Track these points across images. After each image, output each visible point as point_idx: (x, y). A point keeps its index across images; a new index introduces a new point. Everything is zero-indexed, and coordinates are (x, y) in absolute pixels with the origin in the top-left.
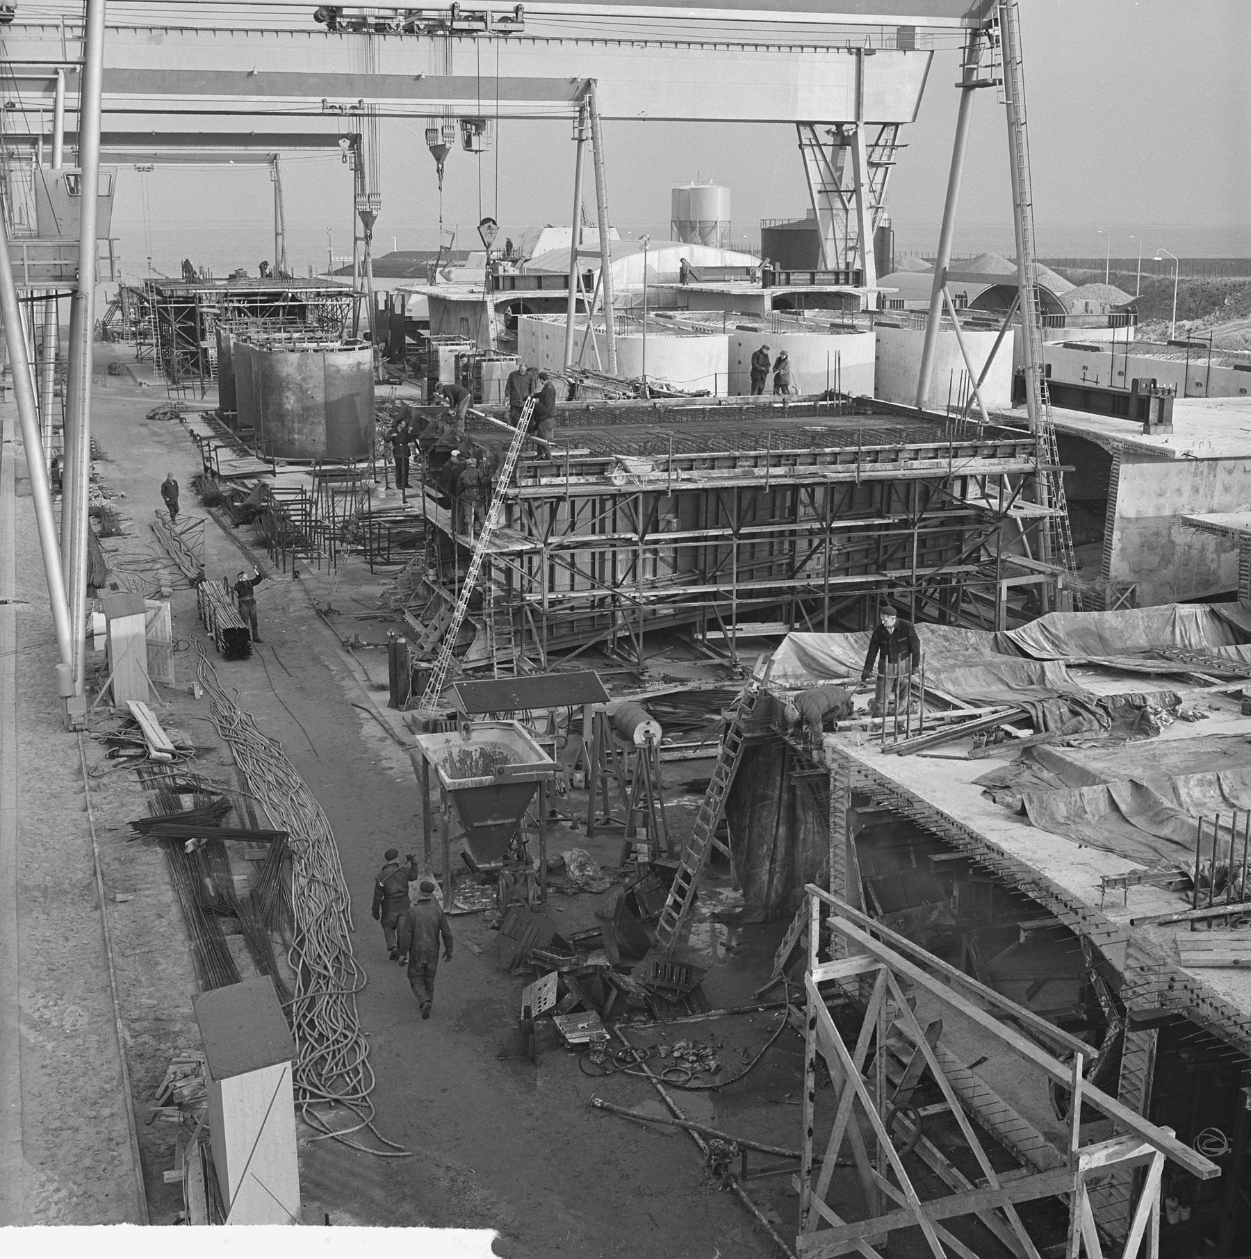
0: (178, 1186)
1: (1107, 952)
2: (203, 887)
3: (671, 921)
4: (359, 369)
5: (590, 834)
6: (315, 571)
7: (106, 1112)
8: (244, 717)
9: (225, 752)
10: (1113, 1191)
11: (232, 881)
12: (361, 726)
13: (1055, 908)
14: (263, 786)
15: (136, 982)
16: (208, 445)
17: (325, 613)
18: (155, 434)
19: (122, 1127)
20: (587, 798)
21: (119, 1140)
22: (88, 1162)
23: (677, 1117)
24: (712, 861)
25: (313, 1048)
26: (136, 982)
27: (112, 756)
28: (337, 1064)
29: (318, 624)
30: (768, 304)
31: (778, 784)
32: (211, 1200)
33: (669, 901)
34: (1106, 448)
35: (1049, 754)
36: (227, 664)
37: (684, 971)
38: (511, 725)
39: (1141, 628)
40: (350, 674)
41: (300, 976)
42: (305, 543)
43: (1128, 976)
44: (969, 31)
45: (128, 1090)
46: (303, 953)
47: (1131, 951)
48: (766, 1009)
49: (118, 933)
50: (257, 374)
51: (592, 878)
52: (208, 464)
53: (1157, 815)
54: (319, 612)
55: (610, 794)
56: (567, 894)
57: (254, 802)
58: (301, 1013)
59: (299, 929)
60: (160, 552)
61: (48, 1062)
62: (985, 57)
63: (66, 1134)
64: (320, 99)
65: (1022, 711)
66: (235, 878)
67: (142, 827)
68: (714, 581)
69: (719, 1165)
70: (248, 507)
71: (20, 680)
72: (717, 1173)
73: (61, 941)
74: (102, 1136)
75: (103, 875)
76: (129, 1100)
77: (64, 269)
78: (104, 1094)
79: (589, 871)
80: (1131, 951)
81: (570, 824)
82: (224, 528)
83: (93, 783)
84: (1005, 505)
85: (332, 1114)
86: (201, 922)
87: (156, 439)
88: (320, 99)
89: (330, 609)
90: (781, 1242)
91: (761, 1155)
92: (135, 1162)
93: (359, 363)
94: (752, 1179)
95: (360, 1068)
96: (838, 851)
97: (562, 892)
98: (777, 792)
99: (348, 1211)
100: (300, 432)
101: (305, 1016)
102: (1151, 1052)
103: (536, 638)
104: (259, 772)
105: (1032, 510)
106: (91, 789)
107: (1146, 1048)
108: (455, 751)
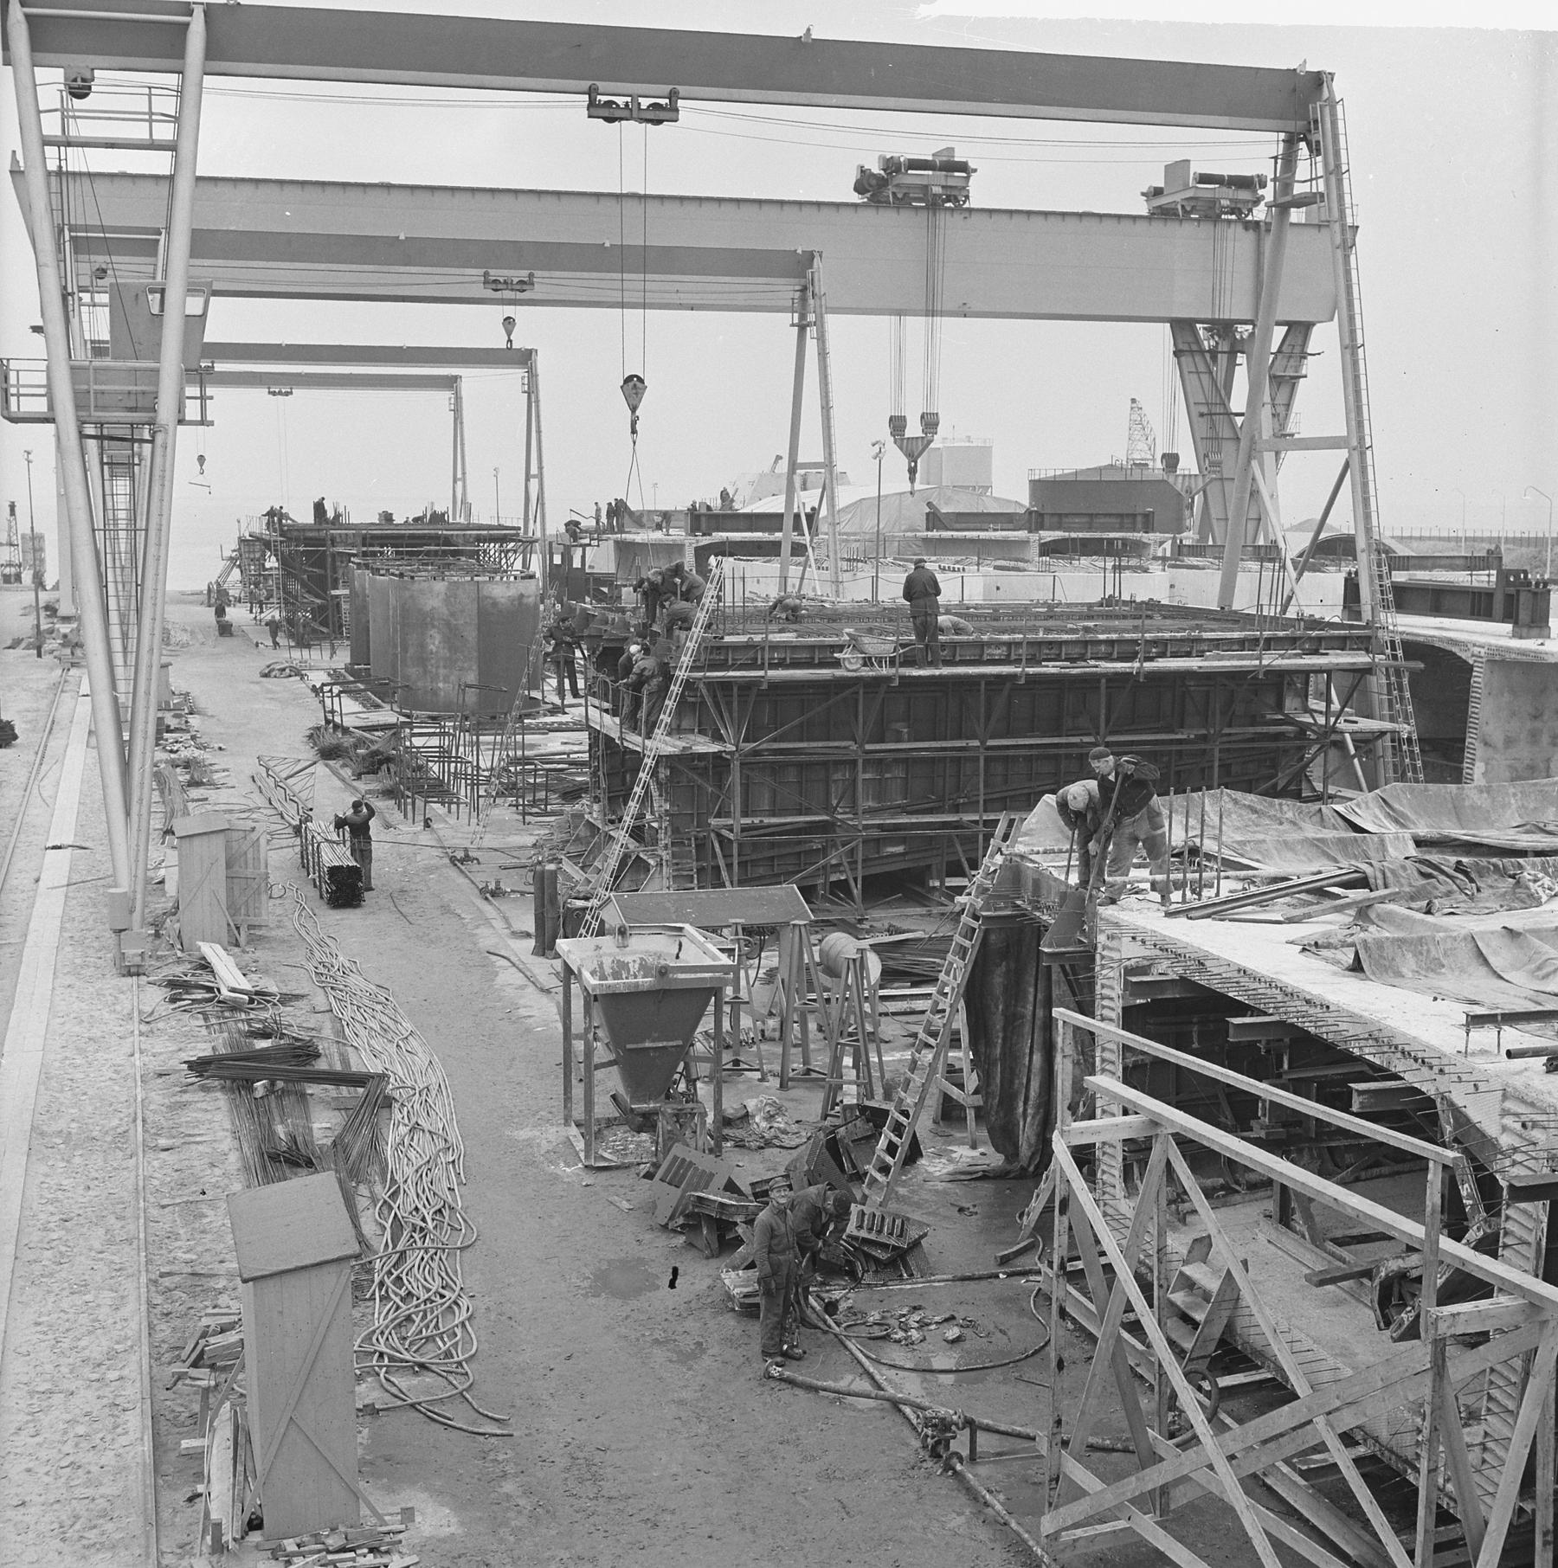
0: (197, 1456)
1: (1474, 1115)
2: (272, 1133)
3: (884, 1169)
4: (520, 604)
5: (783, 1086)
6: (452, 820)
7: (113, 1375)
8: (347, 964)
9: (320, 1001)
10: (1487, 1456)
11: (311, 1129)
12: (497, 974)
13: (1398, 1066)
14: (363, 1033)
15: (173, 1236)
16: (331, 691)
17: (462, 861)
18: (269, 691)
19: (133, 1391)
20: (779, 1050)
21: (126, 1405)
22: (81, 1430)
23: (880, 1388)
24: (943, 1118)
25: (398, 1308)
26: (173, 1236)
27: (173, 1000)
28: (427, 1327)
29: (452, 873)
30: (1035, 550)
31: (1031, 998)
32: (240, 1468)
33: (882, 1143)
34: (1463, 655)
35: (1390, 913)
36: (331, 912)
37: (898, 1222)
38: (681, 929)
39: (1514, 807)
40: (487, 922)
41: (389, 1230)
42: (439, 791)
43: (1505, 1141)
44: (1282, 136)
45: (145, 1349)
46: (395, 1206)
47: (1509, 1105)
48: (1010, 1275)
49: (156, 1182)
50: (395, 609)
51: (785, 1132)
52: (330, 716)
53: (1539, 968)
54: (453, 860)
55: (812, 1046)
56: (749, 1148)
57: (350, 1049)
58: (386, 1269)
59: (393, 1181)
60: (260, 801)
61: (44, 1319)
62: (1303, 170)
63: (57, 1399)
64: (481, 272)
65: (1356, 872)
66: (315, 1126)
67: (200, 1067)
68: (956, 809)
69: (938, 1443)
70: (376, 753)
71: (67, 925)
72: (935, 1455)
73: (80, 1190)
74: (105, 1401)
75: (144, 1121)
76: (145, 1361)
77: (140, 398)
78: (112, 1355)
79: (780, 1123)
80: (1509, 1105)
81: (758, 1075)
82: (343, 780)
83: (144, 1028)
84: (1332, 720)
85: (415, 1381)
86: (264, 1168)
87: (270, 696)
88: (481, 272)
89: (467, 856)
90: (1021, 1530)
91: (997, 1436)
92: (144, 1427)
93: (522, 596)
94: (984, 1463)
95: (458, 1331)
96: (1107, 1055)
97: (744, 1146)
98: (1030, 1007)
99: (426, 1489)
100: (446, 680)
101: (390, 1273)
102: (1539, 1244)
103: (724, 874)
104: (360, 1018)
105: (1365, 724)
106: (141, 1034)
107: (1531, 1239)
108: (607, 962)
